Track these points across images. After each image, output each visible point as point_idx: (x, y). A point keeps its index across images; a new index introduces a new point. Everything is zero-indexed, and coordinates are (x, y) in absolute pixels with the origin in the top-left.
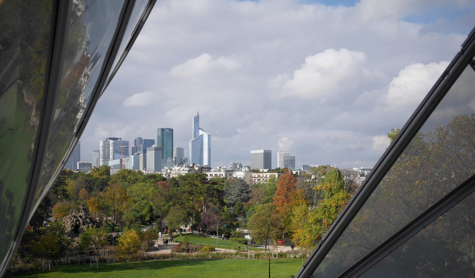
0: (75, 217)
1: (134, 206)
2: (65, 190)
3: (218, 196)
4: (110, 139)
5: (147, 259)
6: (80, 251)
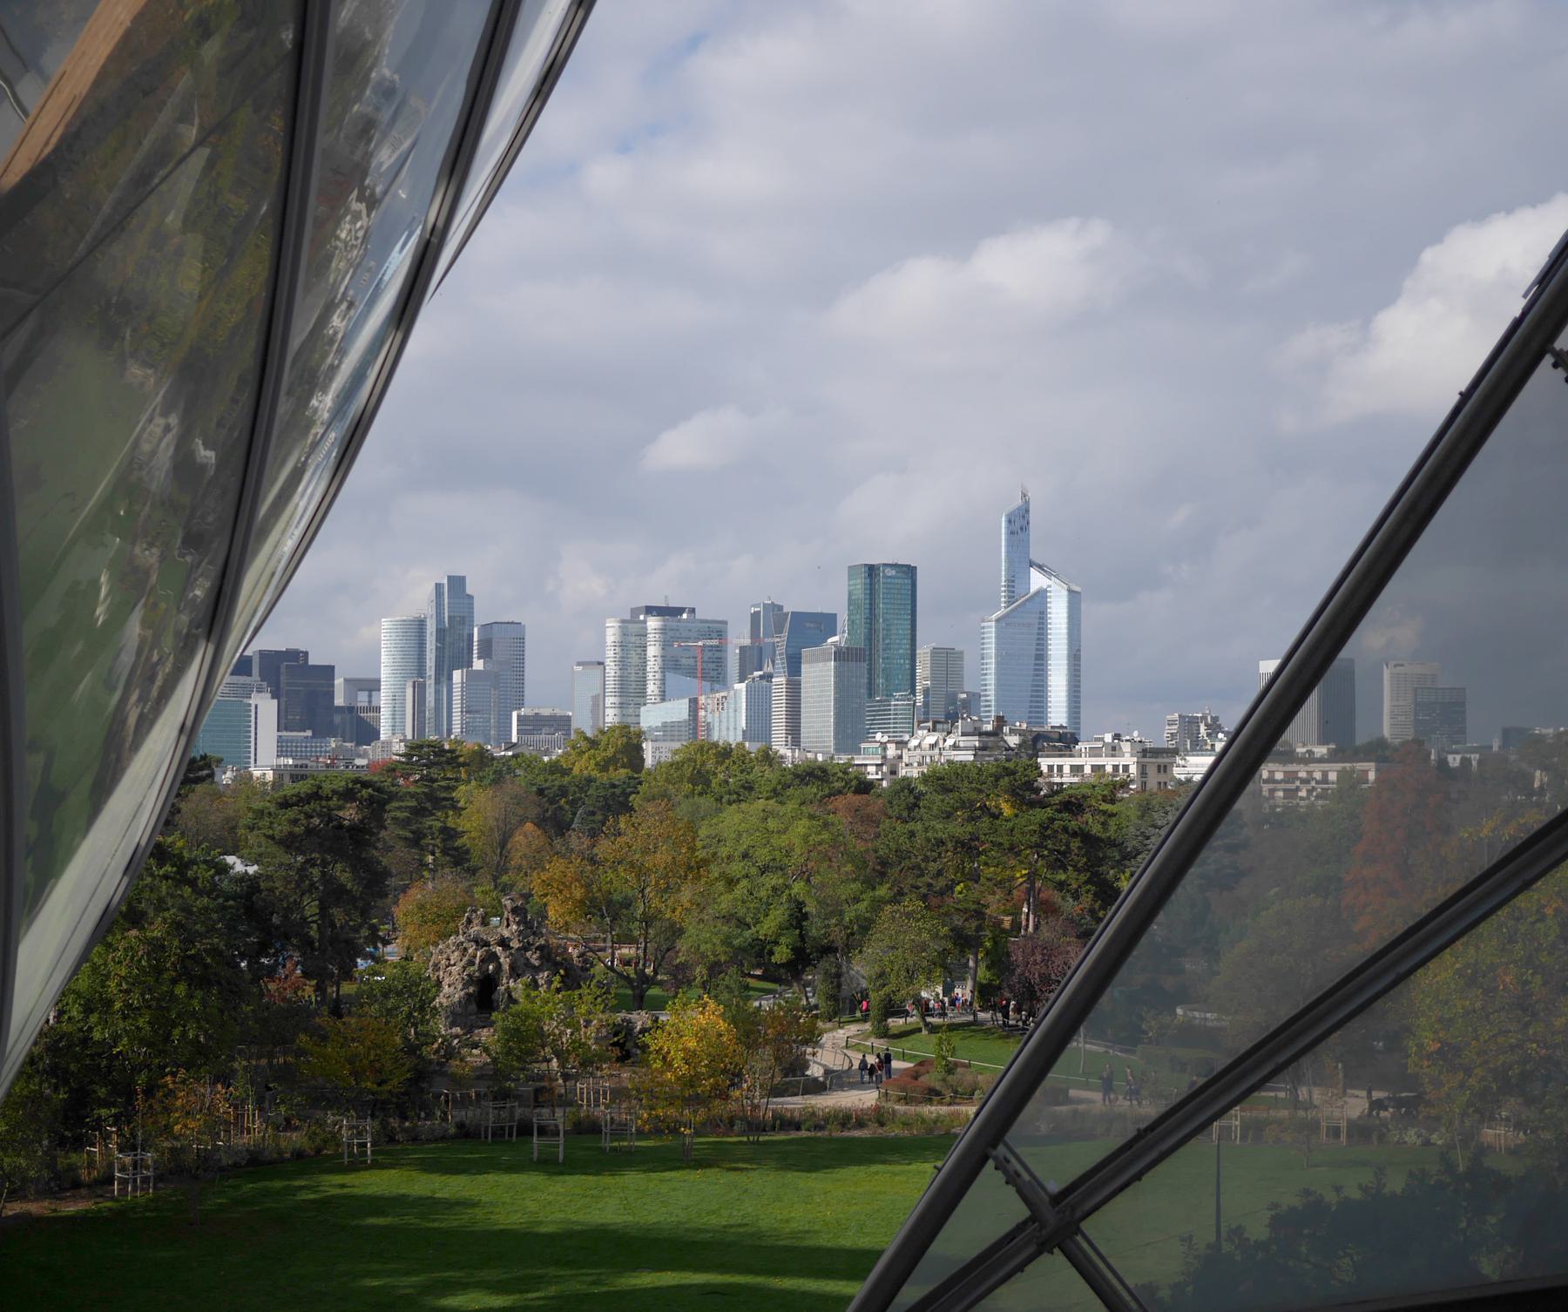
0: (480, 943)
1: (725, 902)
2: (452, 832)
3: (1089, 860)
4: (649, 610)
5: (773, 1128)
6: (496, 1083)
